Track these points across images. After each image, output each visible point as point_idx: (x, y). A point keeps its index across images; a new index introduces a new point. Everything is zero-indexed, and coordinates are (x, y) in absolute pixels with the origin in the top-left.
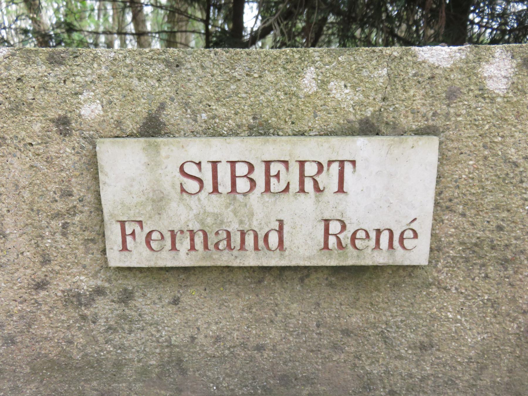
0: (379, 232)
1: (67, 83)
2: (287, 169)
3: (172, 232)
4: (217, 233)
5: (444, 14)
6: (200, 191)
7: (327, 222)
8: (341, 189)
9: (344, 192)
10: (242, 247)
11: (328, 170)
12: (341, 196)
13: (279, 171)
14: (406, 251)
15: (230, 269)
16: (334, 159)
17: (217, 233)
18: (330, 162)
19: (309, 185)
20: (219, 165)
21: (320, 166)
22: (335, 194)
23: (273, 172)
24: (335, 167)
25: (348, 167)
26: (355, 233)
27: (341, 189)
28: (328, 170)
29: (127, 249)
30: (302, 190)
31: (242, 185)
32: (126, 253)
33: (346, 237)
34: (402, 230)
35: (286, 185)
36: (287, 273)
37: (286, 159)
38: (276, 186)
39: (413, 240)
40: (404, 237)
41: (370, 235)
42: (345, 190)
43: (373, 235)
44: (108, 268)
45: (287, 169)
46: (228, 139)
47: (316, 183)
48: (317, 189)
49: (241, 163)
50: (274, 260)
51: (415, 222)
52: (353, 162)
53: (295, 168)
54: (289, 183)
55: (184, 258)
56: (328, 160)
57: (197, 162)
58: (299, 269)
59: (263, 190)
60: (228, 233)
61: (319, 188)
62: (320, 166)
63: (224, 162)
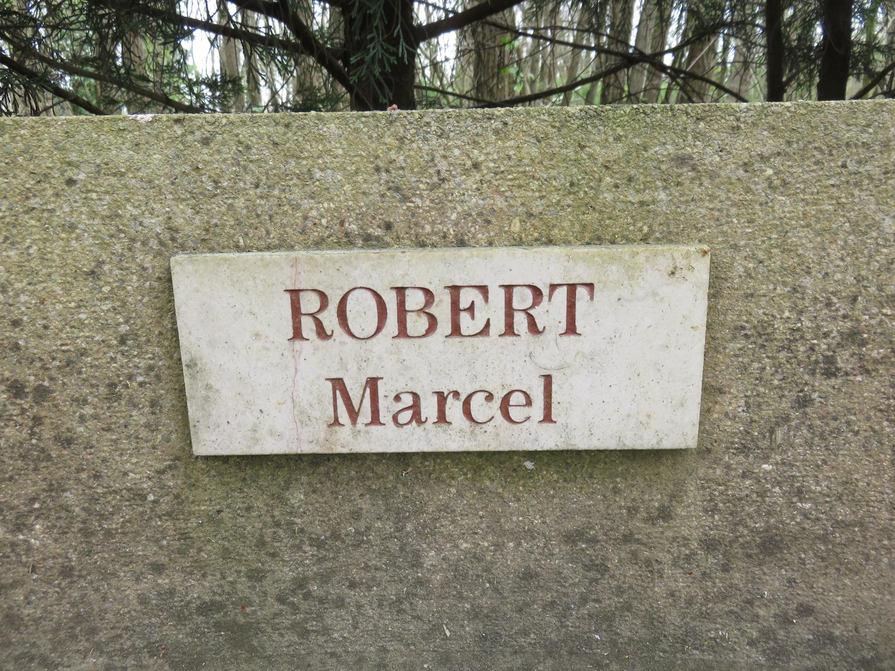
2: (486, 299)
3: (420, 422)
4: (397, 398)
6: (424, 336)
8: (571, 328)
9: (514, 334)
11: (550, 300)
13: (473, 302)
14: (506, 423)
15: (403, 458)
17: (397, 398)
18: (553, 287)
19: (521, 322)
21: (537, 292)
22: (500, 339)
23: (464, 303)
24: (561, 294)
25: (581, 292)
27: (571, 328)
28: (550, 300)
30: (510, 329)
31: (417, 324)
32: (444, 426)
35: (485, 323)
37: (589, 282)
45: (486, 299)
47: (319, 325)
48: (533, 327)
49: (468, 289)
50: (548, 439)
53: (497, 297)
54: (489, 320)
58: (231, 462)
59: (449, 331)
61: (325, 332)
62: (537, 292)
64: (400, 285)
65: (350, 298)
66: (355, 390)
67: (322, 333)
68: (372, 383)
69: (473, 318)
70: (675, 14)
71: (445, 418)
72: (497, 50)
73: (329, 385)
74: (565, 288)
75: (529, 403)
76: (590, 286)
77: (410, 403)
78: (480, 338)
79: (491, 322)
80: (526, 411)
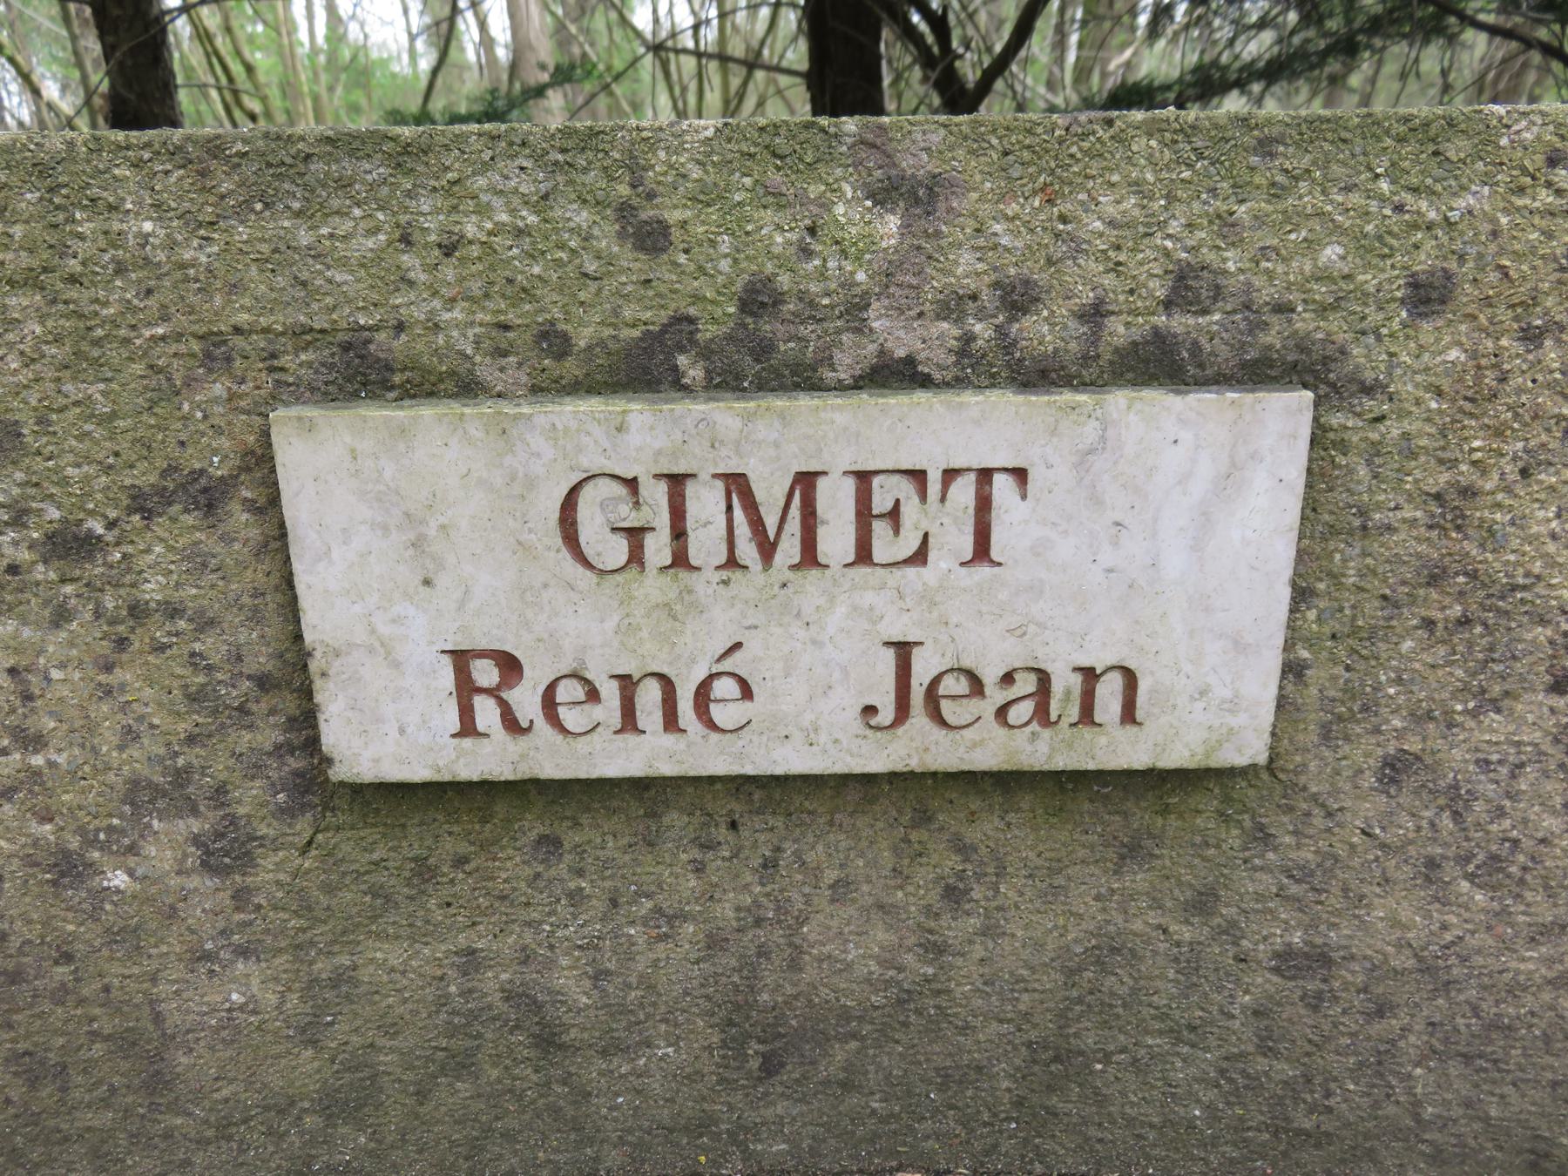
0: (627, 684)
1: (413, 239)
4: (1008, 678)
5: (303, 78)
7: (461, 659)
8: (982, 550)
10: (1087, 714)
11: (943, 499)
12: (983, 572)
13: (898, 501)
16: (965, 466)
18: (950, 475)
20: (690, 489)
22: (964, 570)
23: (881, 503)
24: (964, 492)
25: (1001, 483)
26: (551, 690)
27: (982, 550)
28: (943, 499)
29: (1093, 723)
33: (525, 699)
34: (935, 673)
36: (853, 794)
38: (885, 546)
39: (586, 707)
40: (941, 692)
41: (603, 693)
42: (822, 559)
43: (610, 691)
44: (313, 784)
46: (948, 396)
51: (738, 655)
52: (1020, 474)
54: (926, 535)
55: (983, 746)
56: (945, 467)
57: (630, 476)
60: (1044, 678)
63: (835, 475)
64: (676, 470)
65: (587, 493)
66: (771, 491)
67: (512, 724)
68: (806, 481)
69: (897, 531)
70: (471, 55)
71: (1092, 716)
72: (1107, 25)
73: (720, 484)
74: (972, 476)
75: (593, 695)
76: (1020, 474)
77: (1031, 688)
78: (911, 572)
79: (931, 540)
80: (974, 707)
